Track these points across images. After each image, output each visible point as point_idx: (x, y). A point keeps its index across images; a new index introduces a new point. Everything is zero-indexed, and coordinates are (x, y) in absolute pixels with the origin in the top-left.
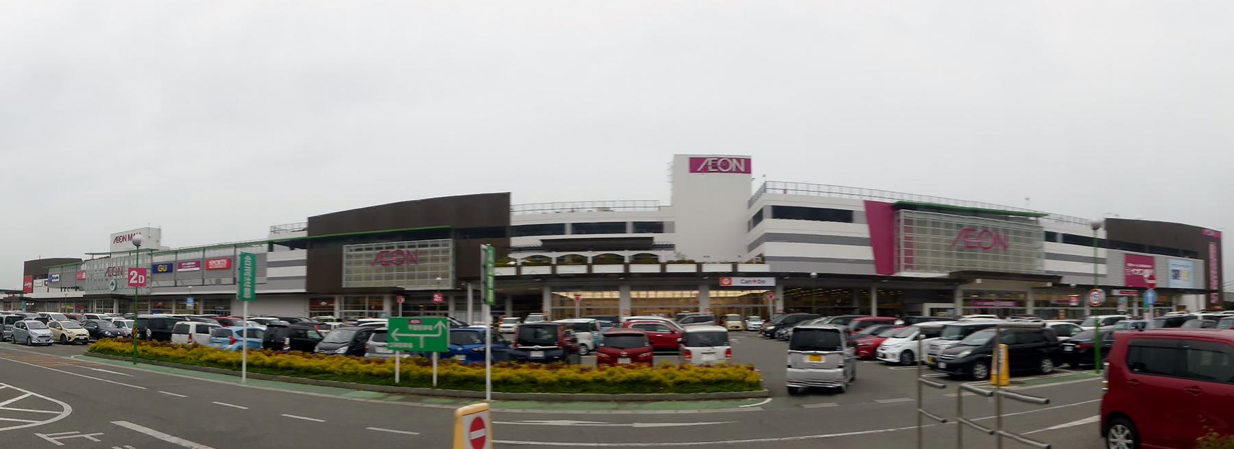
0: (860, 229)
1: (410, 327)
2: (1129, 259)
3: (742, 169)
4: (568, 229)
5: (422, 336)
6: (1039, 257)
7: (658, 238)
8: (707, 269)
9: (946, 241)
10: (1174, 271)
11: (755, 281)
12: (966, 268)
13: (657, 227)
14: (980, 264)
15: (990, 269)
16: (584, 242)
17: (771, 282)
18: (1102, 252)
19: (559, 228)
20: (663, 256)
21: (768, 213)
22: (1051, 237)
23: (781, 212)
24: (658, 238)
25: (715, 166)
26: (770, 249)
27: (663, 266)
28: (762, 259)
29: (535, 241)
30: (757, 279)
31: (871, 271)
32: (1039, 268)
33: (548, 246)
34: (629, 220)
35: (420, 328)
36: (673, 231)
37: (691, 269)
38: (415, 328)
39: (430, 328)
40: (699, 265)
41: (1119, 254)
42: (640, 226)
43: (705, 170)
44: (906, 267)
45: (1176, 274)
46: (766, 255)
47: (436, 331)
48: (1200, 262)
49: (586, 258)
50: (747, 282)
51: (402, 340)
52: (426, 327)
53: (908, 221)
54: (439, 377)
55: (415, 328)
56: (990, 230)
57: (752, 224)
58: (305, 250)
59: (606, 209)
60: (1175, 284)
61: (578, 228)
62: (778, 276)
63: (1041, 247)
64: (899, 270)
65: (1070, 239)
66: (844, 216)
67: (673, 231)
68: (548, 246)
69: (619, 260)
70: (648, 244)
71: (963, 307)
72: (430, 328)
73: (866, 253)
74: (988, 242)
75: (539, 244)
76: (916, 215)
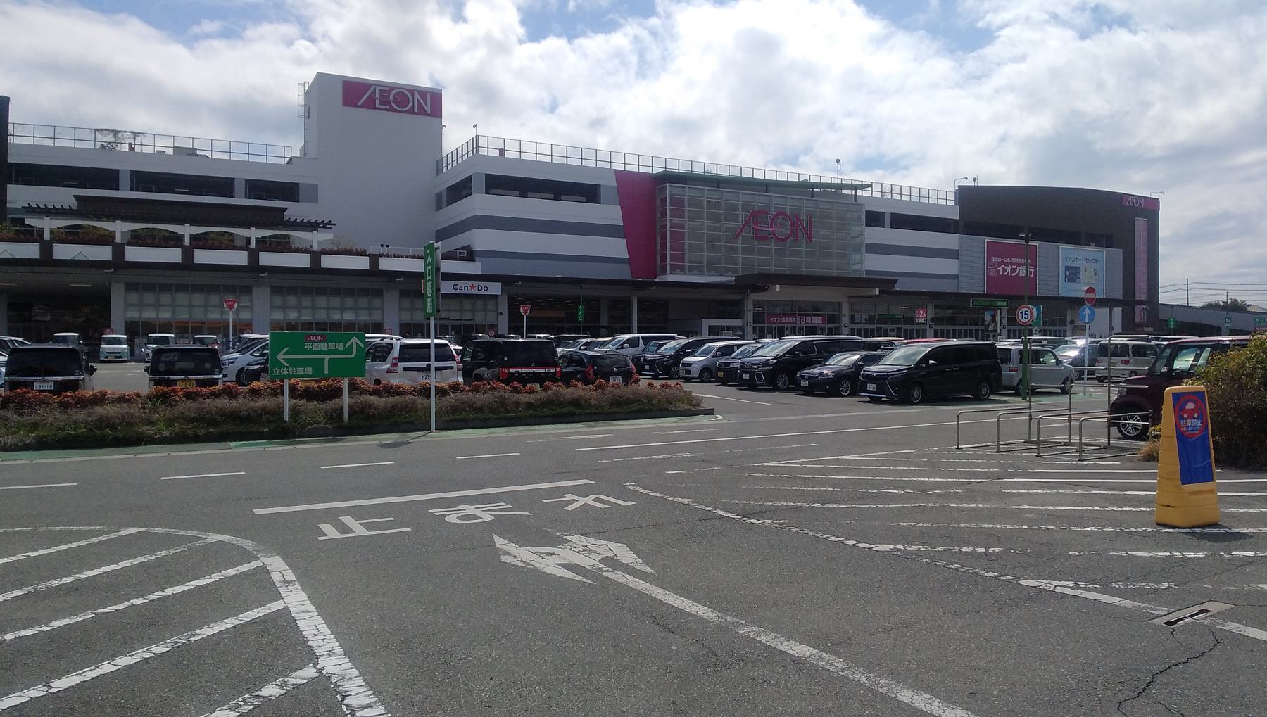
0: (610, 213)
1: (308, 346)
2: (993, 250)
3: (428, 110)
4: (125, 180)
5: (327, 357)
6: (857, 249)
7: (294, 210)
8: (386, 264)
9: (728, 229)
10: (1068, 268)
11: (473, 287)
12: (756, 269)
13: (289, 191)
14: (774, 262)
15: (788, 270)
16: (535, 262)
17: (495, 288)
18: (949, 241)
19: (108, 178)
20: (316, 239)
21: (478, 184)
22: (874, 219)
23: (499, 184)
24: (294, 210)
25: (385, 101)
26: (482, 239)
27: (316, 257)
28: (469, 254)
29: (64, 196)
30: (476, 284)
31: (624, 273)
32: (857, 267)
33: (87, 207)
34: (240, 176)
35: (324, 346)
36: (314, 200)
37: (362, 263)
38: (316, 346)
39: (340, 346)
40: (374, 259)
41: (979, 243)
42: (257, 188)
43: (370, 104)
44: (674, 269)
45: (1073, 274)
46: (476, 247)
47: (349, 351)
48: (1118, 253)
49: (181, 238)
50: (461, 288)
51: (293, 363)
52: (332, 346)
53: (678, 202)
54: (350, 407)
55: (316, 346)
56: (788, 212)
57: (444, 198)
58: (110, 247)
59: (192, 152)
60: (1069, 290)
61: (143, 180)
62: (506, 281)
63: (862, 234)
64: (664, 272)
65: (903, 221)
66: (588, 193)
67: (314, 200)
68: (87, 207)
69: (173, 241)
70: (273, 218)
71: (157, 324)
72: (340, 346)
73: (617, 248)
74: (783, 230)
75: (74, 204)
76: (688, 192)
